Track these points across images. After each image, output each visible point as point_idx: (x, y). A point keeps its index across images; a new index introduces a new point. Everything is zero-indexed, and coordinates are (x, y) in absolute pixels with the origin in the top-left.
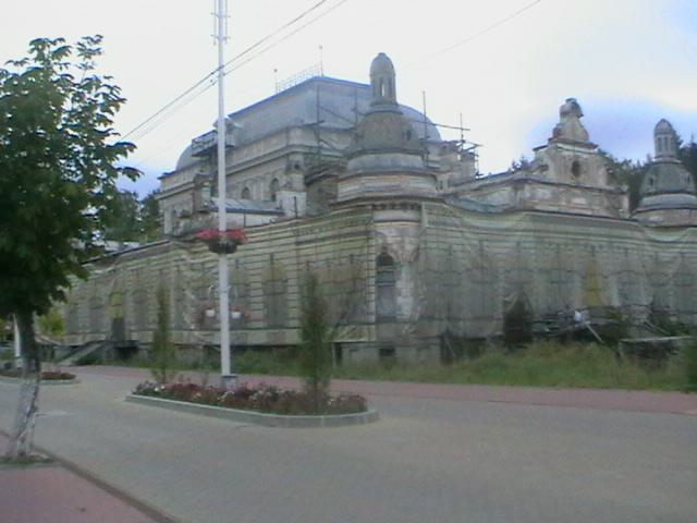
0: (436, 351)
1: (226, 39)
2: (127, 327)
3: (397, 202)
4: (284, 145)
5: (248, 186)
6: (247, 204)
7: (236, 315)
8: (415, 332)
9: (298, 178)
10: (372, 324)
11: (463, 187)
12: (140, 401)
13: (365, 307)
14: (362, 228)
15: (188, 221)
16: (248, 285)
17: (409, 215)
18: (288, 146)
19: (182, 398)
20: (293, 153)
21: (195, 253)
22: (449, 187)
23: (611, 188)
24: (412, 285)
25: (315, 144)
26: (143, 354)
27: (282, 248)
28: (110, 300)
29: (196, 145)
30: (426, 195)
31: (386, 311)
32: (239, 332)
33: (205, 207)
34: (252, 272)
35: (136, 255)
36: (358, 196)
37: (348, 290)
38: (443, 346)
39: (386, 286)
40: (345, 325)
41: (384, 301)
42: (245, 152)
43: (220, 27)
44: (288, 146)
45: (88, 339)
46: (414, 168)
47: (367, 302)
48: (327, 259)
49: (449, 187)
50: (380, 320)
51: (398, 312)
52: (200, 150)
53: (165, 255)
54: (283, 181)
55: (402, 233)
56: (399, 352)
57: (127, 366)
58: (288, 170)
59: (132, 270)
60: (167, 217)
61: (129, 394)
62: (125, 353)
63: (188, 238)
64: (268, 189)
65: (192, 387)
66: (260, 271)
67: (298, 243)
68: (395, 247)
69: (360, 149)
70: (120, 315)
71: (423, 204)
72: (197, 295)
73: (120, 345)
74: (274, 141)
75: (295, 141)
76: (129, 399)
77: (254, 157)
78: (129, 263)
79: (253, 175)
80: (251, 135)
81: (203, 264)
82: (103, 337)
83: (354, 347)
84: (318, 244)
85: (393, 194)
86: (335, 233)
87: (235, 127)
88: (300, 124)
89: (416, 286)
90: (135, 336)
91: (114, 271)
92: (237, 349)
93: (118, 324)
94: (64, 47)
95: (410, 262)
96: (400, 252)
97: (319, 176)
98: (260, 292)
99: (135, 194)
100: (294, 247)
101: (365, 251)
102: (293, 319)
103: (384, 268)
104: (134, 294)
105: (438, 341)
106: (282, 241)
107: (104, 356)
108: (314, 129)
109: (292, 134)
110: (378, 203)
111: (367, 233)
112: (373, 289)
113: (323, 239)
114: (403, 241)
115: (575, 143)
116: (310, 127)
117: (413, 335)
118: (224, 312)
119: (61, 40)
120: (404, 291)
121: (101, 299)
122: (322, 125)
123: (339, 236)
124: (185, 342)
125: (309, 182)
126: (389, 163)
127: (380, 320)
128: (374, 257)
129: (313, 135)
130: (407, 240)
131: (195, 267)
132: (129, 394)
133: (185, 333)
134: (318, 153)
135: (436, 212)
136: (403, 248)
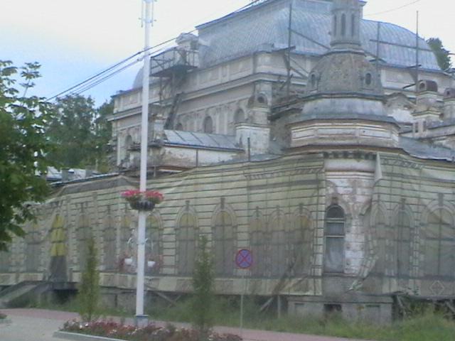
0: (386, 311)
1: (151, 22)
3: (350, 151)
4: (250, 72)
5: (211, 115)
6: (205, 139)
7: (151, 263)
8: (362, 289)
9: (261, 113)
10: (318, 277)
11: (442, 131)
12: (65, 337)
13: (312, 261)
14: (313, 177)
16: (197, 228)
17: (363, 164)
18: (255, 74)
19: (101, 334)
20: (259, 81)
22: (424, 130)
24: (362, 238)
25: (284, 71)
27: (233, 192)
28: (49, 236)
30: (385, 145)
31: (333, 265)
33: (156, 141)
34: (201, 215)
35: (82, 186)
36: (311, 142)
38: (395, 305)
39: (335, 238)
40: (293, 277)
41: (332, 254)
42: (210, 75)
43: (147, 11)
44: (255, 74)
45: (21, 279)
46: (372, 114)
47: (314, 254)
48: (278, 207)
49: (424, 130)
50: (327, 274)
51: (347, 267)
52: (160, 69)
53: (112, 190)
54: (246, 113)
55: (354, 184)
56: (345, 309)
57: (65, 310)
58: (251, 102)
59: (76, 204)
60: (121, 142)
61: (57, 330)
62: (63, 295)
65: (112, 325)
67: (250, 188)
68: (346, 198)
69: (315, 92)
70: (61, 253)
71: (378, 153)
73: (58, 287)
74: (241, 65)
75: (262, 68)
76: (56, 335)
78: (73, 196)
79: (217, 102)
80: (217, 55)
82: (40, 277)
83: (300, 301)
84: (268, 190)
85: (347, 142)
86: (286, 179)
87: (200, 45)
88: (270, 49)
89: (367, 241)
91: (57, 203)
92: (152, 295)
93: (58, 263)
94: (13, 68)
95: (361, 215)
96: (351, 204)
97: (283, 112)
100: (245, 191)
101: (315, 200)
103: (332, 220)
104: (77, 230)
105: (390, 300)
106: (233, 185)
107: (39, 300)
108: (285, 55)
109: (260, 59)
110: (330, 151)
111: (318, 181)
112: (321, 241)
113: (275, 185)
114: (354, 192)
117: (360, 292)
118: (140, 260)
119: (9, 62)
120: (354, 245)
121: (40, 234)
123: (290, 184)
125: (273, 118)
126: (345, 109)
127: (327, 274)
128: (323, 207)
129: (283, 62)
130: (359, 191)
132: (57, 330)
134: (288, 83)
135: (390, 162)
136: (354, 199)
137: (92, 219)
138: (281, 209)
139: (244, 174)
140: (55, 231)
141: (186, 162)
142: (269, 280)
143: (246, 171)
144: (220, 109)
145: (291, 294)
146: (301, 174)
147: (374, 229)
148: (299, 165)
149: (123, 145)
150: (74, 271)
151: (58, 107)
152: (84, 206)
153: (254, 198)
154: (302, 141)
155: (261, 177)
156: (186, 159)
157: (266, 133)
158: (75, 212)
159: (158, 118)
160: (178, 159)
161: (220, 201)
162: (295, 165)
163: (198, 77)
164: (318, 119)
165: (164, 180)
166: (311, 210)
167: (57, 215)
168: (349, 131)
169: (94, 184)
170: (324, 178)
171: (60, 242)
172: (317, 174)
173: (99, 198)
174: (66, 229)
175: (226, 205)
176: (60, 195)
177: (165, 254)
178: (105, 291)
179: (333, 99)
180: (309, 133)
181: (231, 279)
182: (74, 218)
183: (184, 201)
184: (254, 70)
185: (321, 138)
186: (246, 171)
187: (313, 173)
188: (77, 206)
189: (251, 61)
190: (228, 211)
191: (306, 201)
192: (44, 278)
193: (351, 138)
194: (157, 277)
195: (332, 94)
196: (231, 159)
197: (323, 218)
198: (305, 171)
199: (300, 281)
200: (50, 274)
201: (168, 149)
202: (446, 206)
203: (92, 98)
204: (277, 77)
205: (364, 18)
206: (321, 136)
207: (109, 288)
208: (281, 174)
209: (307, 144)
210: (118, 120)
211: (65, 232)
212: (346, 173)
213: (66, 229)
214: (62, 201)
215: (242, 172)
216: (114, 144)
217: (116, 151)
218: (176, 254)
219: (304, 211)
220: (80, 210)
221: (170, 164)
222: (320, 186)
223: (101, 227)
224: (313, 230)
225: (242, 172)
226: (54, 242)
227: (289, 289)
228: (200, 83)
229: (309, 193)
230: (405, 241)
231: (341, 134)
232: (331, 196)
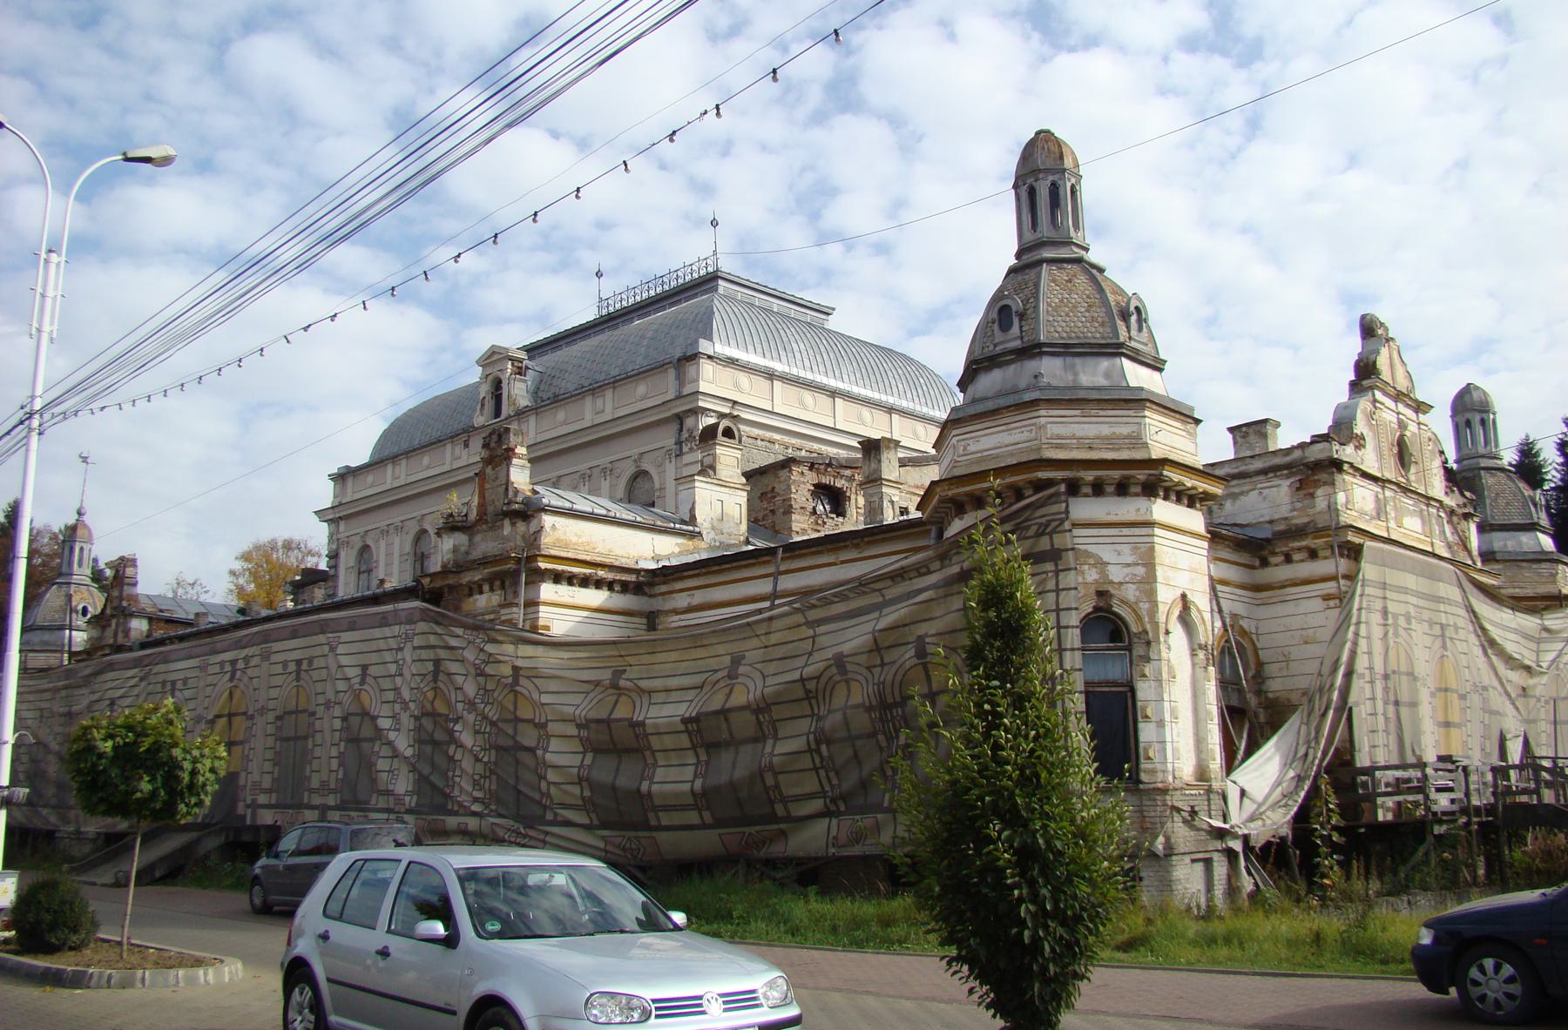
4: (670, 395)
5: (369, 542)
15: (461, 539)
23: (1450, 501)
59: (285, 664)
64: (408, 547)
68: (1130, 592)
69: (1017, 344)
77: (446, 468)
78: (276, 646)
85: (1124, 455)
104: (279, 718)
115: (1398, 396)
128: (1074, 619)
149: (352, 564)
152: (305, 666)
154: (997, 457)
158: (278, 680)
168: (1125, 430)
172: (1050, 534)
179: (1069, 360)
180: (1026, 436)
182: (274, 693)
189: (672, 373)
193: (1132, 447)
195: (1066, 346)
196: (677, 550)
197: (1077, 643)
212: (1126, 531)
220: (294, 676)
221: (553, 552)
231: (1107, 438)
232: (1092, 590)
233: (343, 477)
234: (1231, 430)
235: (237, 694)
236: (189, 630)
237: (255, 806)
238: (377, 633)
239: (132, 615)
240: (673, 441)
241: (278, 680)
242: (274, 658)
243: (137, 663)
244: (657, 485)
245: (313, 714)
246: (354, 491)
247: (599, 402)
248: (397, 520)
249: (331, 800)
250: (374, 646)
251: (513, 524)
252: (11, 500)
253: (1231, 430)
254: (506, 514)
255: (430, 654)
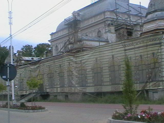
2: (45, 87)
5: (100, 30)
9: (113, 28)
14: (158, 42)
15: (72, 45)
21: (77, 57)
26: (51, 97)
29: (66, 21)
32: (98, 87)
36: (156, 28)
37: (152, 68)
42: (86, 22)
52: (67, 23)
59: (47, 66)
63: (73, 51)
66: (107, 62)
67: (125, 50)
69: (153, 10)
70: (41, 83)
72: (78, 73)
78: (45, 63)
81: (81, 61)
86: (145, 44)
90: (48, 90)
91: (39, 66)
98: (108, 71)
99: (31, 46)
100: (124, 52)
101: (160, 51)
102: (103, 84)
106: (118, 50)
109: (106, 14)
111: (160, 43)
116: (113, 11)
122: (117, 10)
124: (73, 92)
129: (114, 15)
131: (77, 62)
133: (73, 88)
137: (53, 70)
138: (142, 56)
139: (122, 45)
140: (39, 76)
141: (91, 46)
142: (138, 84)
143: (123, 44)
144: (91, 32)
145: (151, 88)
146: (152, 41)
147: (150, 65)
148: (151, 38)
150: (47, 88)
151: (24, 48)
153: (127, 54)
154: (151, 29)
155: (131, 45)
156: (91, 45)
157: (114, 35)
158: (46, 69)
159: (79, 32)
160: (88, 45)
161: (112, 57)
162: (149, 38)
163: (81, 23)
164: (159, 19)
165: (85, 52)
166: (158, 55)
167: (39, 71)
169: (54, 58)
170: (163, 42)
171: (41, 79)
173: (56, 63)
174: (43, 75)
175: (115, 58)
176: (40, 64)
177: (104, 77)
178: (61, 94)
181: (119, 85)
182: (46, 71)
183: (95, 58)
184: (104, 17)
185: (160, 26)
186: (123, 44)
187: (158, 40)
188: (47, 67)
189: (103, 14)
190: (116, 60)
191: (156, 52)
192: (36, 91)
194: (86, 87)
195: (161, 10)
198: (155, 40)
199: (155, 83)
200: (38, 90)
201: (85, 42)
202: (143, 58)
203: (32, 45)
204: (112, 19)
205: (130, 3)
206: (160, 26)
207: (62, 93)
208: (142, 43)
209: (153, 29)
210: (52, 41)
211: (43, 76)
213: (43, 75)
214: (41, 66)
215: (121, 45)
216: (52, 49)
217: (52, 51)
218: (110, 76)
219: (155, 55)
220: (48, 68)
222: (161, 45)
223: (57, 72)
224: (160, 63)
225: (121, 45)
226: (39, 79)
227: (150, 87)
228: (82, 25)
229: (157, 48)
230: (158, 68)
233: (52, 34)
234: (50, 35)
235: (40, 71)
236: (31, 62)
237: (46, 89)
238: (60, 59)
239: (22, 60)
240: (104, 26)
241: (46, 69)
242: (45, 65)
243: (24, 68)
244: (102, 33)
245: (53, 73)
246: (54, 37)
247: (92, 19)
248: (61, 41)
249: (58, 86)
250: (61, 61)
251: (79, 43)
252: (10, 46)
253: (50, 35)
254: (78, 41)
255: (68, 61)
